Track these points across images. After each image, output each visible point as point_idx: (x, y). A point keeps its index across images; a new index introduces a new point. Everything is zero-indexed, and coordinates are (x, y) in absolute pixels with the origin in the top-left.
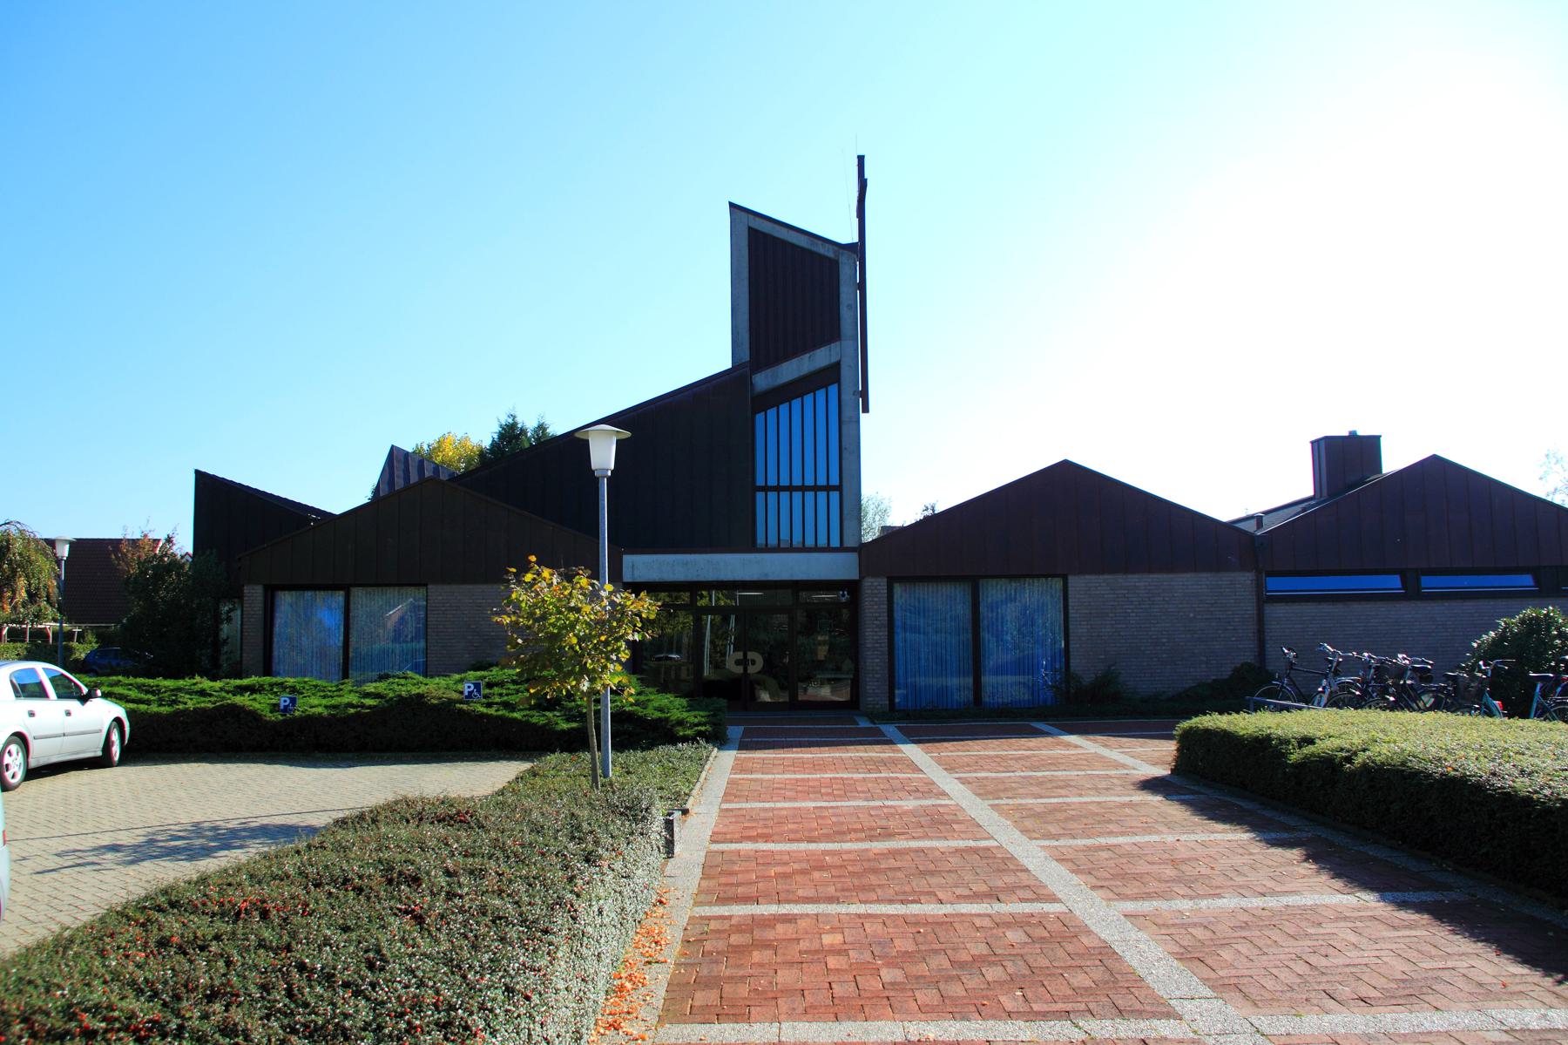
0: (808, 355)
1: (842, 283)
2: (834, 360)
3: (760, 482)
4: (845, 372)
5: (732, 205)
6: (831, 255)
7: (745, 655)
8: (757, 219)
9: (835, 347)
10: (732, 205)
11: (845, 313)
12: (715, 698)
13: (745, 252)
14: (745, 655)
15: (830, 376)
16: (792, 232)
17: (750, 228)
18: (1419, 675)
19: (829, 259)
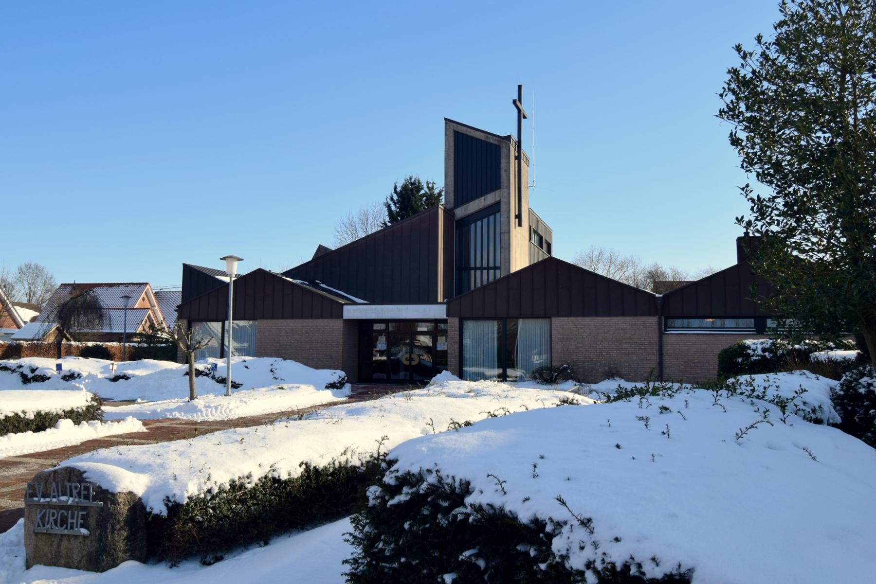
0: (483, 198)
1: (502, 158)
2: (497, 199)
3: (472, 265)
4: (503, 206)
5: (446, 119)
6: (496, 143)
7: (410, 363)
8: (458, 126)
9: (498, 192)
10: (446, 119)
11: (503, 174)
12: (226, 420)
13: (452, 144)
14: (410, 363)
15: (495, 209)
16: (476, 132)
17: (455, 131)
18: (791, 74)
19: (496, 146)
